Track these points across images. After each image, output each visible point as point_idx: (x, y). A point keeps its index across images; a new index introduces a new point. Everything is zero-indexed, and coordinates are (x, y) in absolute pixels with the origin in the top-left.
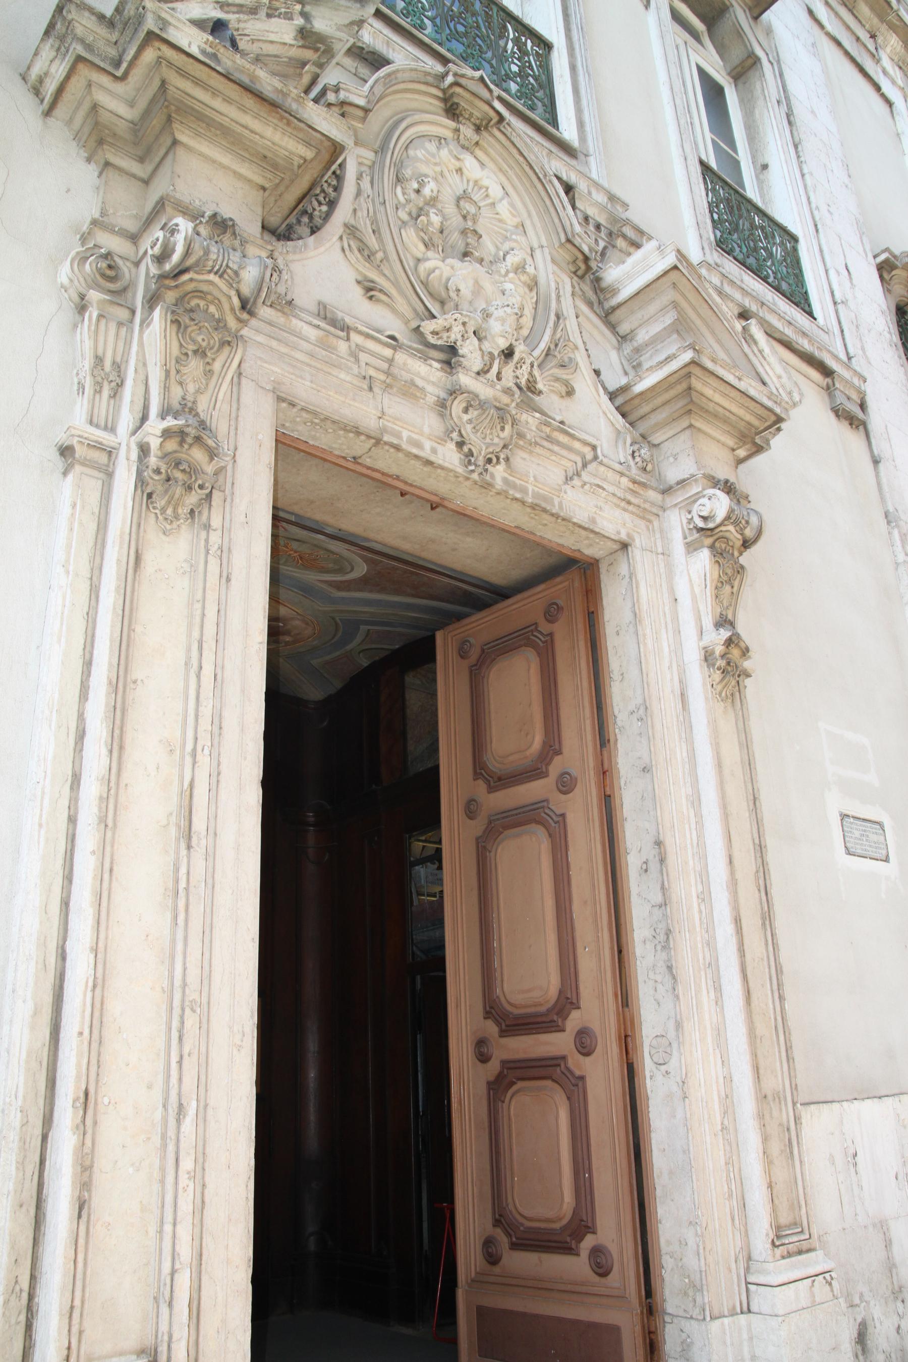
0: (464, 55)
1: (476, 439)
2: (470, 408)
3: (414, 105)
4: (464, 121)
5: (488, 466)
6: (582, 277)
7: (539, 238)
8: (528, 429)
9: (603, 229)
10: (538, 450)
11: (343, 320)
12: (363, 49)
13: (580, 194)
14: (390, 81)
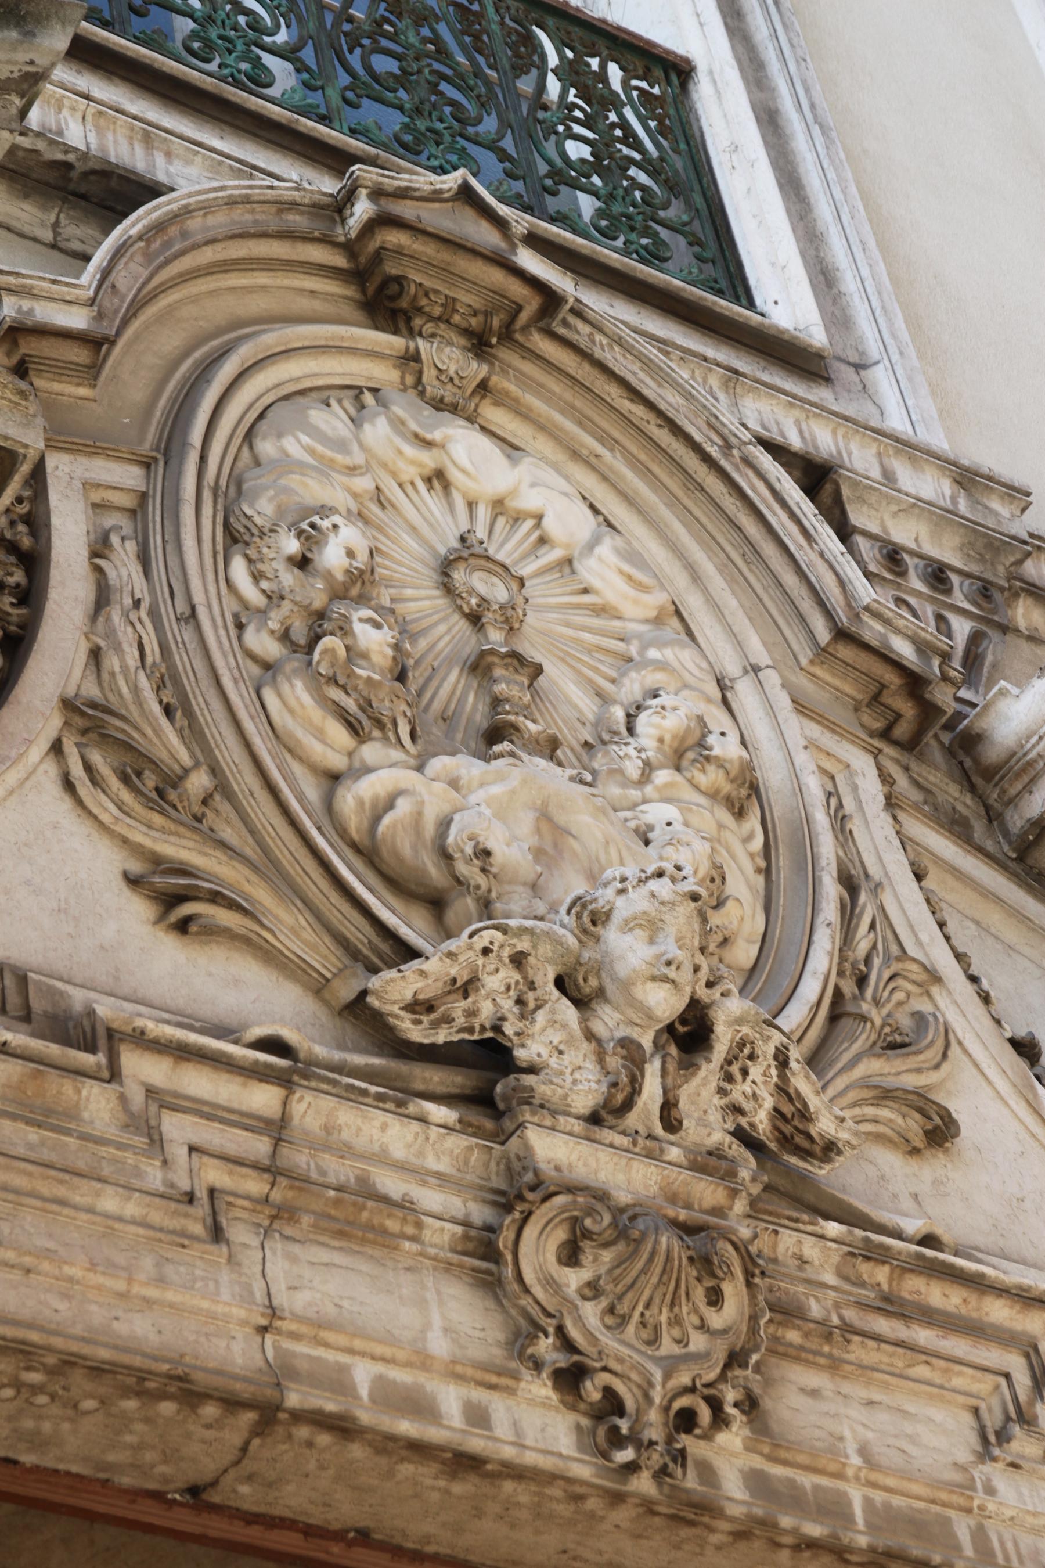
0: (408, 138)
1: (625, 1351)
2: (586, 1245)
3: (257, 305)
4: (429, 328)
5: (685, 1440)
6: (911, 745)
7: (739, 644)
8: (808, 1282)
9: (955, 579)
10: (859, 1351)
11: (91, 1013)
12: (68, 166)
13: (856, 484)
14: (167, 245)
